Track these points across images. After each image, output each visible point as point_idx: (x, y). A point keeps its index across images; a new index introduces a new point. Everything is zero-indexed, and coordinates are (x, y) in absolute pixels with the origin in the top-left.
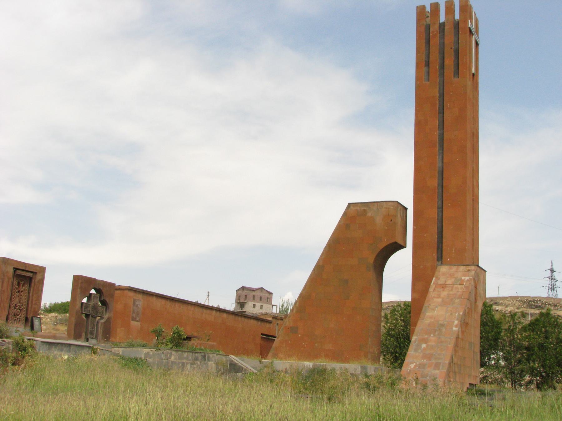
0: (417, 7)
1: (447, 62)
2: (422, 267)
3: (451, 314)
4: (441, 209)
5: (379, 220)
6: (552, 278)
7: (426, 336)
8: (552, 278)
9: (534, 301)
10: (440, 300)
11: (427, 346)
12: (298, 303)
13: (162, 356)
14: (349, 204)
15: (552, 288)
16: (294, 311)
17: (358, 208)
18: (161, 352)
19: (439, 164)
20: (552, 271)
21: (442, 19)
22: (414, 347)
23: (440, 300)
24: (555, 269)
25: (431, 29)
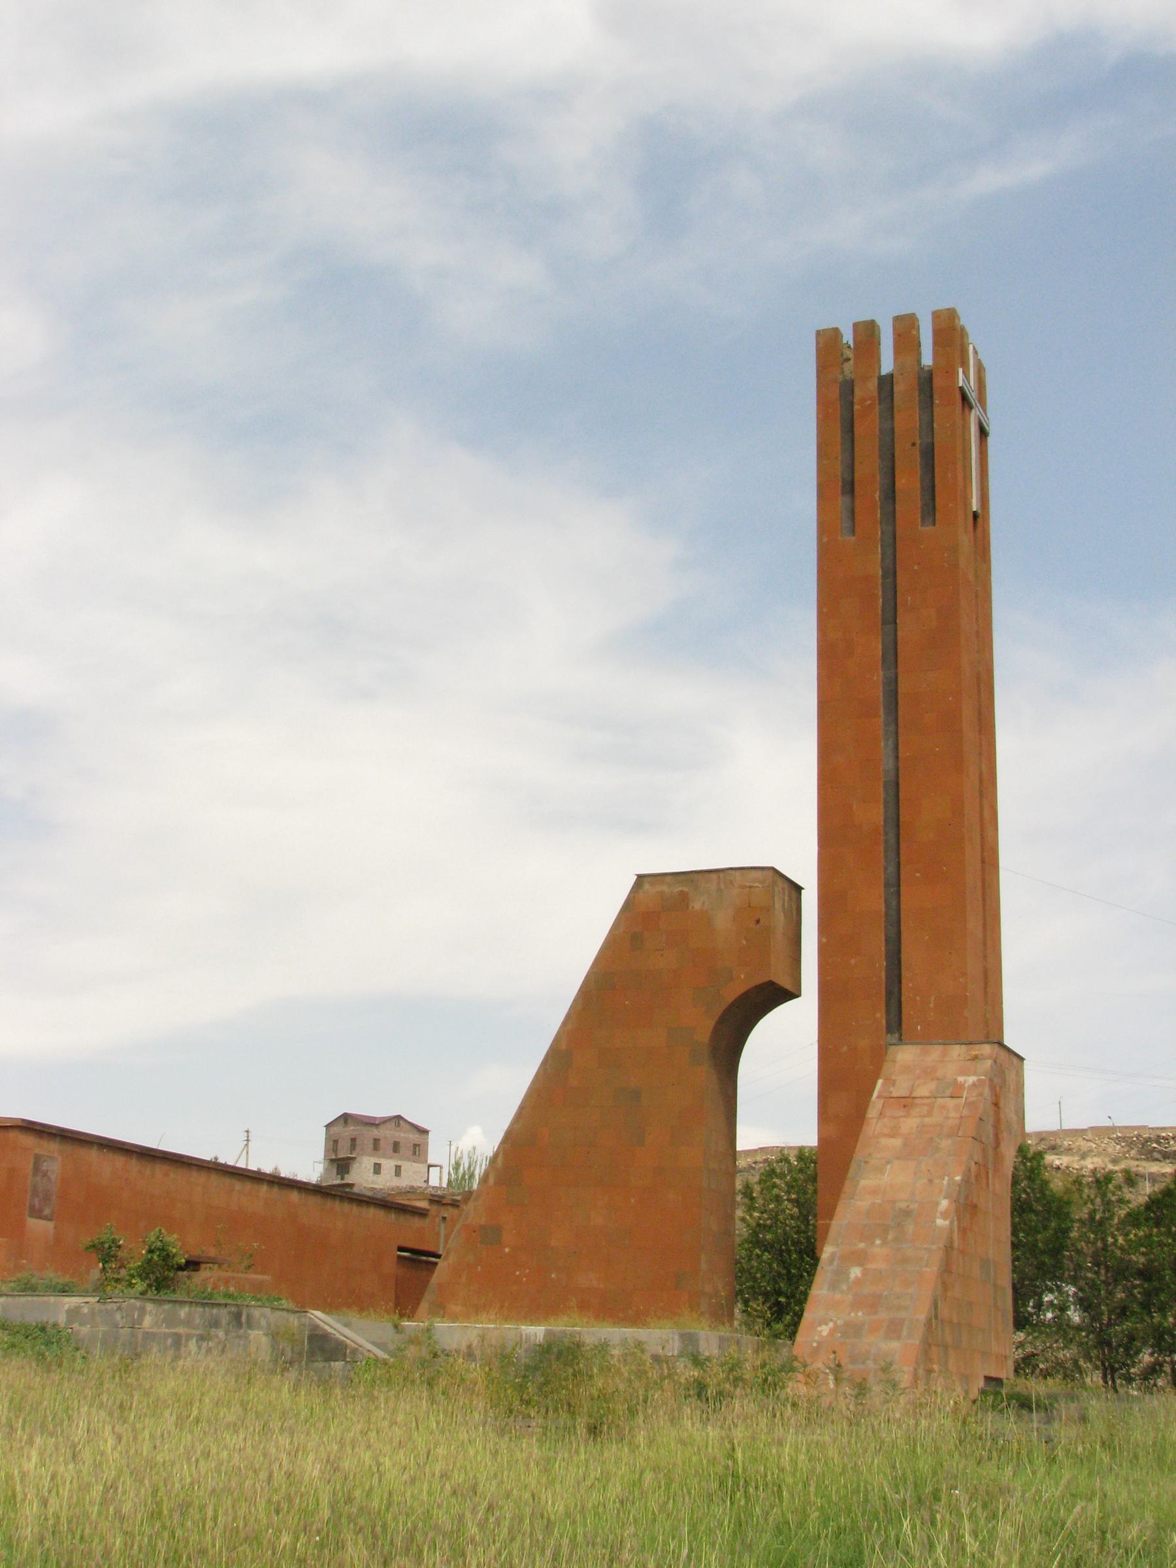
2: (845, 1049)
3: (931, 1181)
4: (894, 886)
5: (723, 920)
7: (862, 1245)
9: (1158, 1139)
10: (897, 1142)
11: (865, 1273)
14: (640, 877)
16: (491, 1181)
17: (665, 888)
18: (115, 1306)
21: (887, 365)
23: (897, 1142)
25: (858, 393)
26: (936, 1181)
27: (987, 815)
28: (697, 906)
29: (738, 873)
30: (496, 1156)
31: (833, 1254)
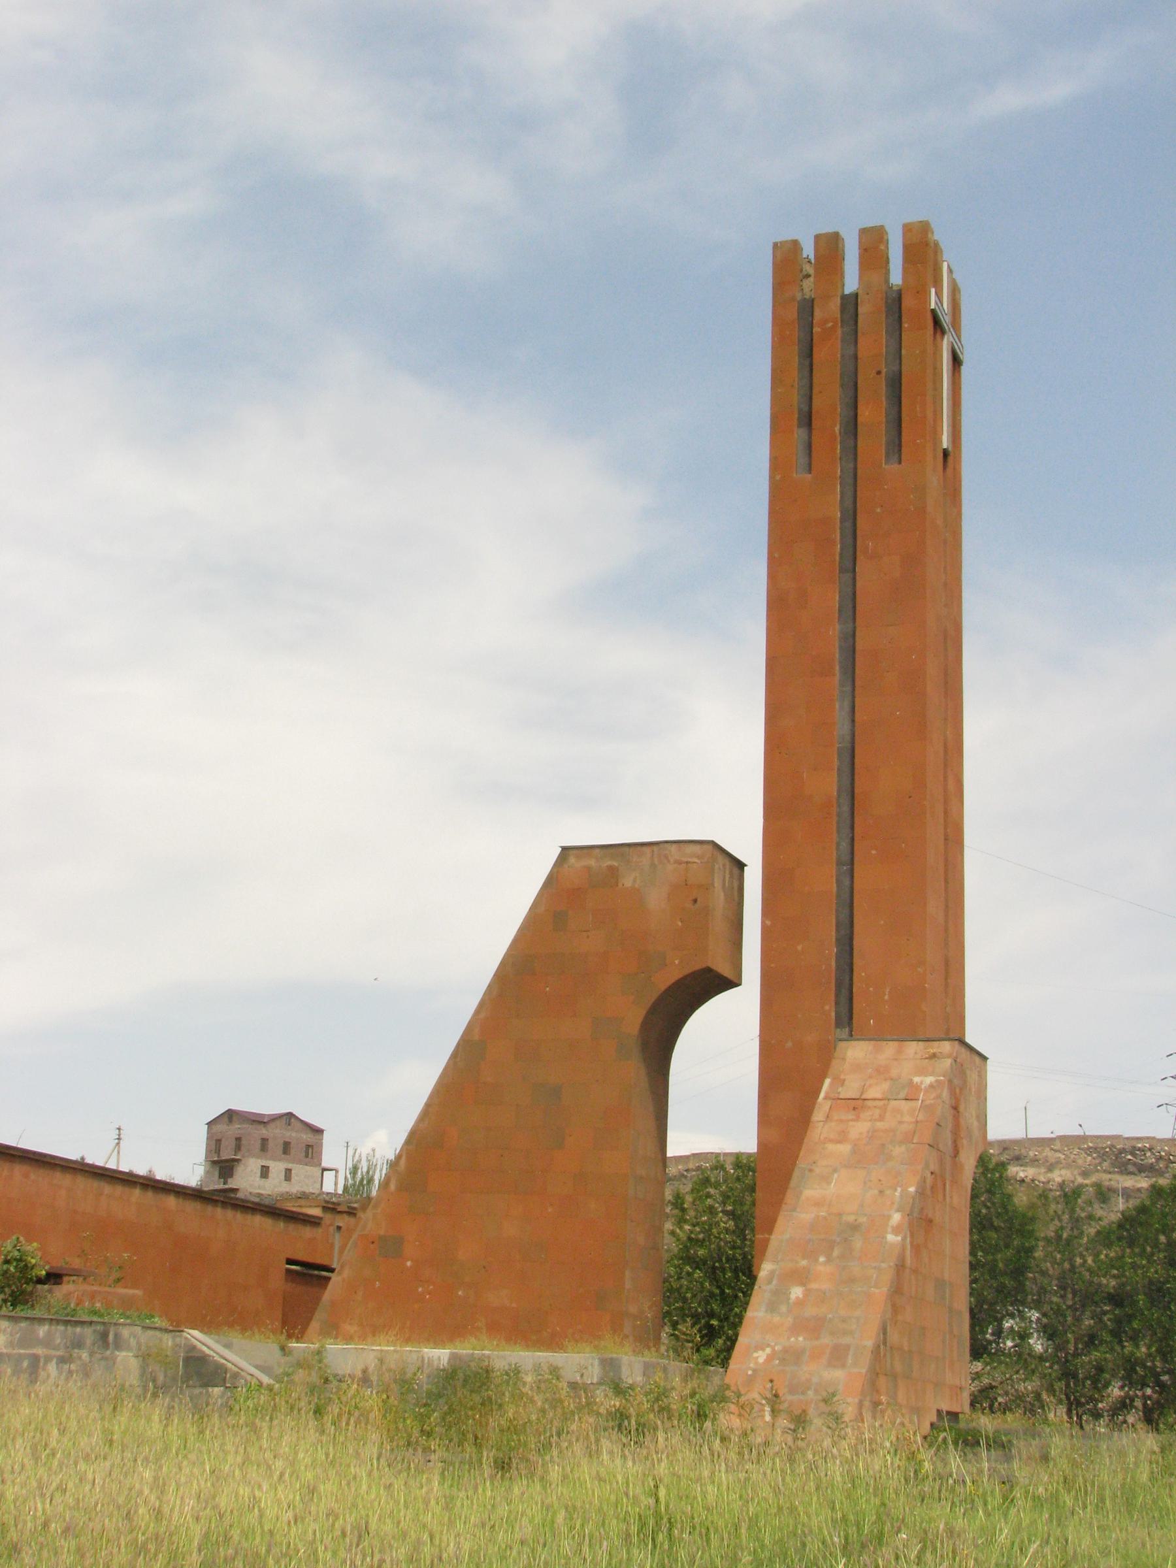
1: (866, 414)
2: (789, 1044)
3: (881, 1192)
5: (656, 899)
7: (804, 1263)
9: (1133, 1151)
10: (845, 1149)
12: (403, 1162)
16: (392, 1187)
17: (592, 862)
21: (851, 283)
23: (845, 1149)
25: (818, 314)
26: (888, 1192)
31: (772, 1273)
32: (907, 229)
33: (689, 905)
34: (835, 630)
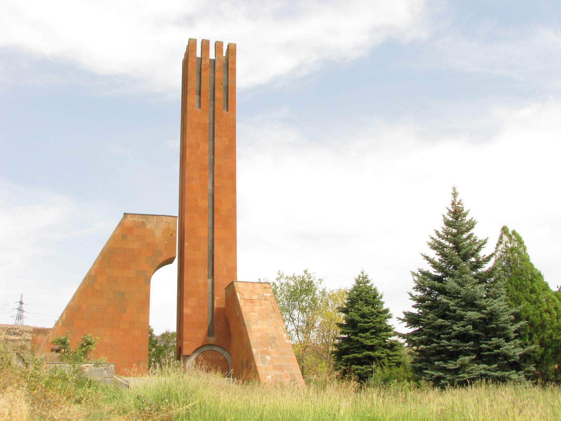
0: (190, 39)
1: (217, 95)
2: (194, 283)
5: (158, 233)
6: (20, 310)
7: (265, 349)
8: (20, 310)
9: (12, 329)
11: (271, 357)
12: (64, 316)
13: (105, 372)
15: (20, 317)
16: (60, 324)
17: (136, 219)
18: (103, 368)
19: (210, 187)
20: (21, 303)
21: (212, 56)
22: (259, 359)
24: (23, 302)
25: (203, 63)
27: (222, 208)
28: (149, 227)
29: (164, 217)
30: (63, 314)
32: (203, 41)
33: (169, 236)
34: (208, 158)
